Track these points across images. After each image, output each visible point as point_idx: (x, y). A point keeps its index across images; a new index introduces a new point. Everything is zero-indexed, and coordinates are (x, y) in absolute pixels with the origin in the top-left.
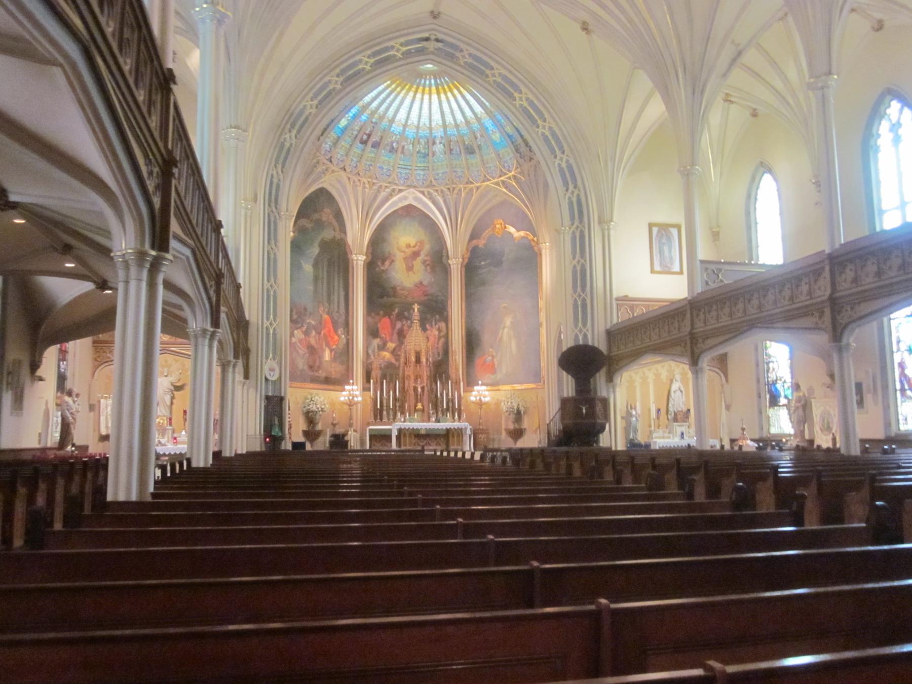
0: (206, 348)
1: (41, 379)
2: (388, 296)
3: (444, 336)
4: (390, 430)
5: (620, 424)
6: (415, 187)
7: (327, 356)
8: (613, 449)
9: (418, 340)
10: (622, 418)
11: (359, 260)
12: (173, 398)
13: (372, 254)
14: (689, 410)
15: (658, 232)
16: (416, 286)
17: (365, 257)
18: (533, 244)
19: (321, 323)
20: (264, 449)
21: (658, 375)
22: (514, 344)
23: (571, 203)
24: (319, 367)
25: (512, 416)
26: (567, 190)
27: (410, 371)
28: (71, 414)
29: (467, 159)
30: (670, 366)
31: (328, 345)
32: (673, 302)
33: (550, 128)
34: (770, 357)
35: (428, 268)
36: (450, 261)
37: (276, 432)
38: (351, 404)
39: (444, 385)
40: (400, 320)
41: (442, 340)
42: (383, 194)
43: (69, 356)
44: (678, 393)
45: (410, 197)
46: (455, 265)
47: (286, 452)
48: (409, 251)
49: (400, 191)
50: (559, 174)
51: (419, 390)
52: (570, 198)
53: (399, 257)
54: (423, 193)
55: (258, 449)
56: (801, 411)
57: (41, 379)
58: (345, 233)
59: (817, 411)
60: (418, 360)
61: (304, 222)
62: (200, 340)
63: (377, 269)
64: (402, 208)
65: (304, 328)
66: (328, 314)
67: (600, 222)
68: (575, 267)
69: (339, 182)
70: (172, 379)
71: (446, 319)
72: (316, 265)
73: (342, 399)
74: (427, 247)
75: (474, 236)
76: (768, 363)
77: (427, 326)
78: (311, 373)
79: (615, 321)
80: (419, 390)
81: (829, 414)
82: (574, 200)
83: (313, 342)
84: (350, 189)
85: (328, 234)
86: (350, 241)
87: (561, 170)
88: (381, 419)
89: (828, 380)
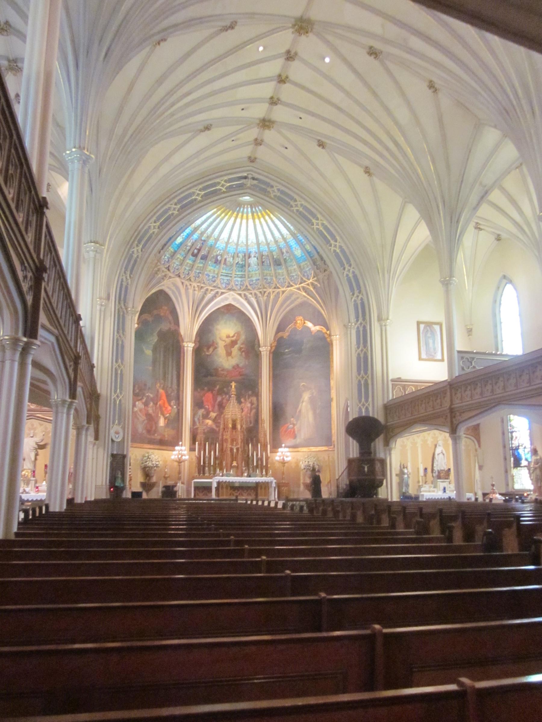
0: (65, 415)
3: (254, 408)
4: (211, 483)
6: (234, 290)
7: (162, 422)
8: (390, 500)
10: (397, 475)
11: (189, 347)
12: (37, 455)
13: (199, 342)
14: (449, 469)
15: (424, 328)
16: (234, 367)
17: (193, 345)
18: (326, 336)
19: (157, 395)
20: (108, 497)
24: (155, 431)
27: (228, 436)
29: (275, 270)
30: (435, 434)
35: (243, 353)
36: (260, 349)
37: (118, 483)
38: (180, 462)
39: (255, 448)
40: (221, 394)
41: (254, 411)
42: (209, 296)
44: (441, 455)
46: (265, 351)
47: (127, 500)
48: (228, 341)
49: (222, 293)
50: (347, 283)
51: (235, 450)
52: (355, 301)
53: (221, 345)
54: (240, 295)
55: (104, 497)
60: (234, 427)
61: (145, 316)
62: (60, 409)
65: (144, 400)
66: (163, 389)
67: (380, 319)
68: (359, 354)
70: (37, 439)
71: (257, 394)
72: (155, 350)
74: (243, 337)
75: (280, 328)
76: (512, 432)
77: (242, 400)
78: (148, 436)
80: (235, 450)
82: (359, 302)
83: (151, 411)
84: (183, 291)
86: (182, 331)
88: (204, 473)
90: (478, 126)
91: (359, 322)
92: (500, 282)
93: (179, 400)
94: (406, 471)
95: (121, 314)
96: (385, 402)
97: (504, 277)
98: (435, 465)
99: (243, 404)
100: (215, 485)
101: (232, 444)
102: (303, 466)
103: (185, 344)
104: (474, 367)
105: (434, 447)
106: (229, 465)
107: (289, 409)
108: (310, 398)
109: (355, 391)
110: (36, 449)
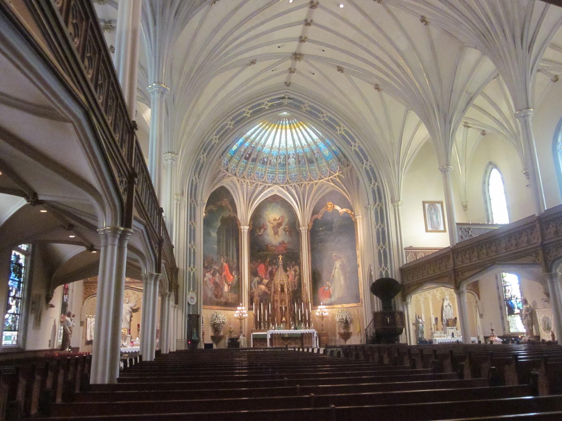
0: (152, 286)
1: (52, 306)
2: (263, 251)
4: (266, 335)
5: (412, 328)
6: (278, 184)
7: (226, 288)
9: (282, 278)
10: (413, 324)
11: (245, 229)
12: (131, 317)
13: (253, 225)
14: (456, 318)
18: (351, 216)
19: (222, 268)
20: (187, 348)
21: (434, 296)
22: (342, 278)
23: (373, 191)
25: (343, 325)
26: (371, 183)
27: (277, 297)
28: (70, 328)
29: (309, 167)
31: (226, 282)
32: (441, 250)
33: (359, 147)
34: (506, 282)
35: (287, 233)
37: (194, 337)
39: (299, 305)
40: (271, 265)
41: (297, 277)
42: (259, 189)
43: (70, 292)
44: (448, 307)
45: (276, 190)
46: (304, 230)
47: (201, 350)
48: (275, 223)
49: (269, 187)
52: (373, 188)
53: (270, 227)
54: (283, 187)
55: (183, 348)
56: (529, 318)
57: (52, 306)
58: (236, 213)
59: (540, 317)
60: (282, 290)
62: (149, 281)
63: (256, 234)
64: (270, 197)
65: (212, 272)
66: (226, 262)
67: (393, 201)
68: (378, 229)
69: (232, 182)
70: (132, 304)
72: (218, 233)
73: (236, 315)
75: (315, 212)
77: (288, 269)
78: (216, 300)
79: (405, 262)
81: (548, 319)
82: (376, 189)
83: (217, 280)
85: (226, 214)
86: (239, 217)
87: (367, 172)
88: (260, 328)
89: (545, 297)
90: (462, 48)
91: (377, 204)
92: (488, 166)
93: (238, 270)
94: (421, 321)
95: (193, 206)
96: (401, 266)
97: (491, 163)
98: (444, 315)
99: (289, 272)
100: (269, 337)
101: (281, 304)
102: (338, 320)
103: (242, 227)
104: (471, 236)
105: (442, 300)
106: (280, 320)
107: (325, 275)
108: (340, 265)
109: (377, 258)
110: (131, 312)
